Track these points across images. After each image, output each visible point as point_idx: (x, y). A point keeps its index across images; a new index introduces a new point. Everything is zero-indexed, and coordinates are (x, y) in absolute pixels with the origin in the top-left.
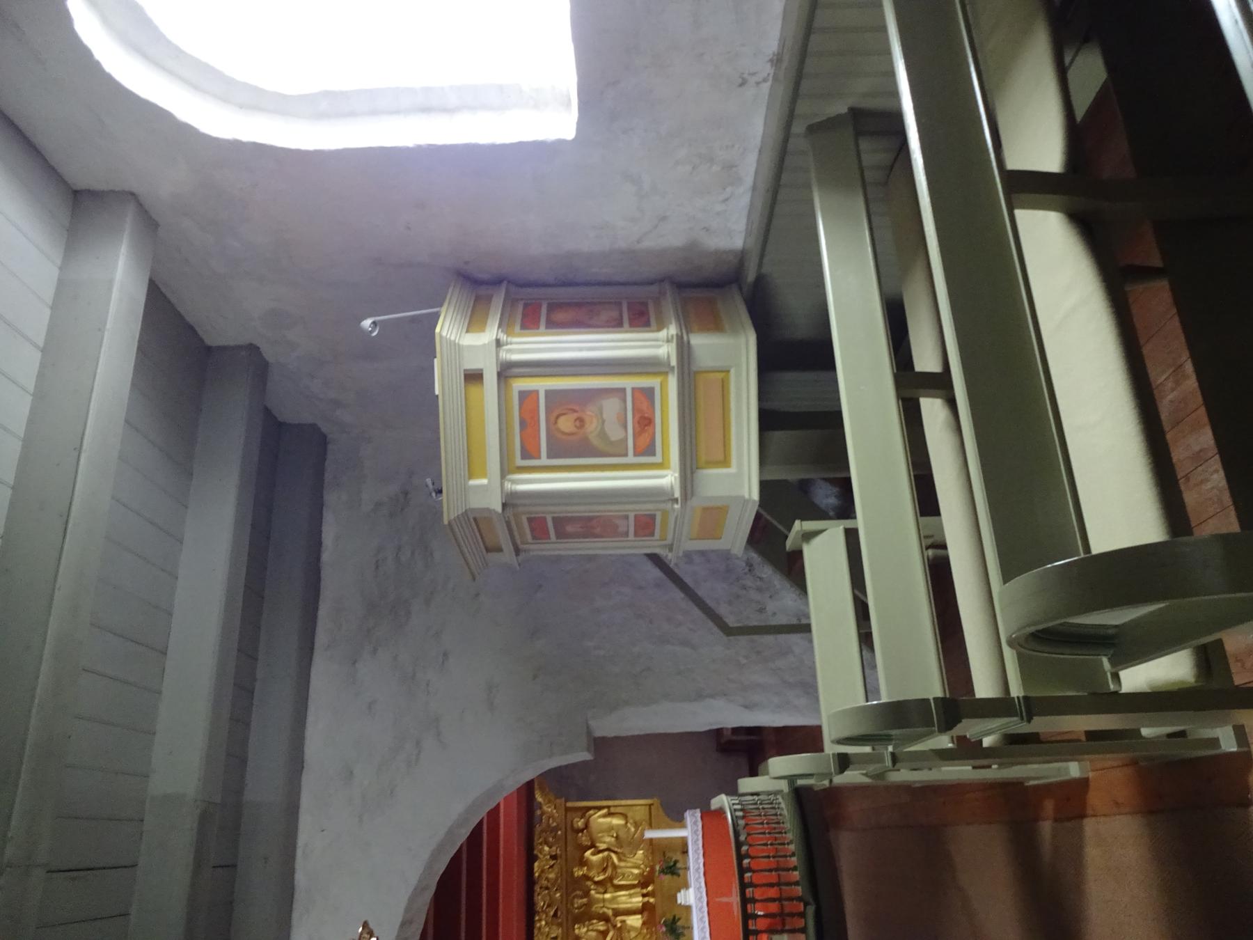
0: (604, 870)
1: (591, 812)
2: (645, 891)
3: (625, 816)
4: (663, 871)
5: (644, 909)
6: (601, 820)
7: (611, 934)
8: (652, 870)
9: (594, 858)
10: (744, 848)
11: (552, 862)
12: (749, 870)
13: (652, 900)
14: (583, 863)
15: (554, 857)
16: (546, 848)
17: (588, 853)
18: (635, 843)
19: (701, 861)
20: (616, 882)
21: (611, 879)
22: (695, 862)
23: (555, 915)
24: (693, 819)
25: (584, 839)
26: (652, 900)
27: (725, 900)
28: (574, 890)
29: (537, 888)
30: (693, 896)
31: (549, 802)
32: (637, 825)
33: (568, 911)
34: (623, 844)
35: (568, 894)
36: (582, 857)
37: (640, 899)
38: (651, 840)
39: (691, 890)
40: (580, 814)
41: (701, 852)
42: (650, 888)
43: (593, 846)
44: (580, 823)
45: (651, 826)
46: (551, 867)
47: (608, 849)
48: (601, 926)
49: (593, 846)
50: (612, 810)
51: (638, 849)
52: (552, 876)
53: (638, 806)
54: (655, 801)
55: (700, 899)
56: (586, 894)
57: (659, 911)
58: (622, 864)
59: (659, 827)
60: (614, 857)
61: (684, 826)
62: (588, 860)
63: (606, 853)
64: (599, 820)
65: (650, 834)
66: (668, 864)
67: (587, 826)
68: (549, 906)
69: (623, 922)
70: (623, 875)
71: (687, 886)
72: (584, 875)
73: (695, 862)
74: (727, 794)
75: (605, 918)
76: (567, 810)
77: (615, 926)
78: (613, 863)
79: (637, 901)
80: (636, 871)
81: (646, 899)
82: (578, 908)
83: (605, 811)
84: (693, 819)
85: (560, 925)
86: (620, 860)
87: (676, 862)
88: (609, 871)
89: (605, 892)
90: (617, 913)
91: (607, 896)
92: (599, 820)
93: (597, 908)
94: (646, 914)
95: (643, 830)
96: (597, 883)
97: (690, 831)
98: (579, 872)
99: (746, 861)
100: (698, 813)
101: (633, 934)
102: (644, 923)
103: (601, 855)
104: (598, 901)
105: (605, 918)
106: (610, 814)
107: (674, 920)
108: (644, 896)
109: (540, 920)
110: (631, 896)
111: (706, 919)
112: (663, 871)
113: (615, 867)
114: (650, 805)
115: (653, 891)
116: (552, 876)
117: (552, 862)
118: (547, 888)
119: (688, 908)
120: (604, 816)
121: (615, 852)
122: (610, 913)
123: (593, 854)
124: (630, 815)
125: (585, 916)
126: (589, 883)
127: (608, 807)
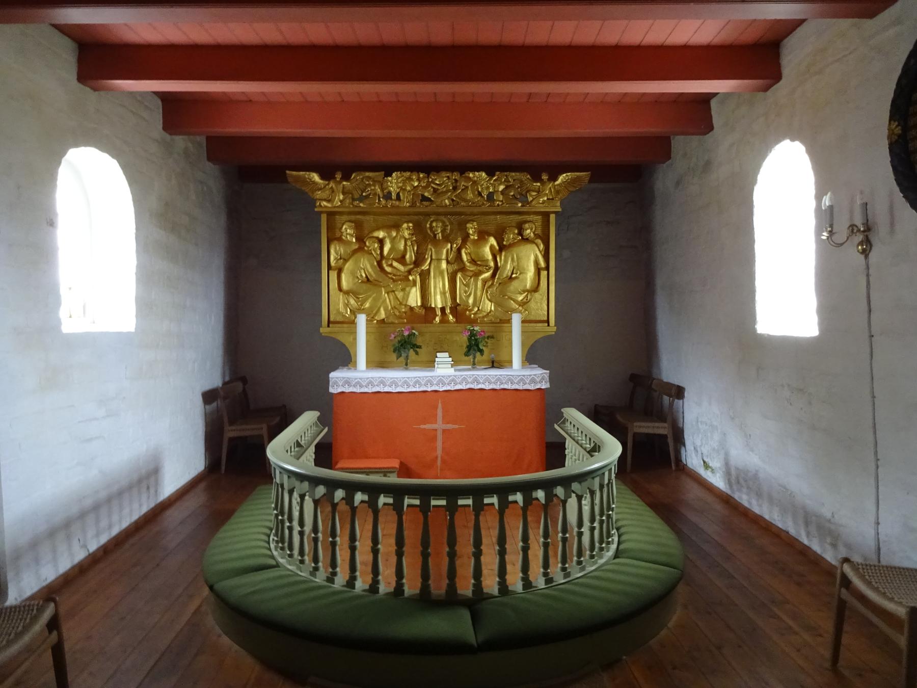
0: (473, 262)
1: (542, 247)
2: (448, 311)
3: (535, 289)
4: (472, 334)
5: (428, 310)
6: (532, 258)
7: (401, 268)
8: (473, 322)
9: (487, 250)
10: (540, 494)
11: (485, 194)
12: (504, 504)
13: (437, 319)
14: (483, 235)
15: (490, 196)
16: (502, 188)
17: (492, 241)
18: (500, 300)
19: (487, 386)
20: (459, 275)
21: (463, 269)
22: (484, 378)
23: (425, 199)
24: (537, 378)
25: (511, 236)
26: (437, 319)
27: (449, 426)
28: (451, 223)
29: (456, 175)
30: (445, 373)
31: (558, 192)
32: (523, 304)
33: (428, 215)
34: (500, 283)
35: (446, 214)
36: (490, 235)
37: (440, 306)
38: (509, 321)
39: (451, 371)
40: (539, 232)
41: (497, 387)
42: (451, 317)
43: (502, 248)
44: (528, 232)
45: (523, 322)
46: (480, 194)
47: (497, 268)
48: (410, 256)
49: (502, 248)
50: (544, 274)
51: (498, 304)
52: (470, 195)
53: (544, 305)
54: (552, 328)
55: (441, 382)
56: (447, 239)
57: (424, 327)
58: (480, 284)
59: (524, 332)
60: (487, 275)
61: (523, 366)
62: (486, 241)
63: (492, 264)
64: (529, 257)
65: (516, 319)
66: (479, 345)
67: (526, 240)
68: (435, 190)
69: (414, 283)
70: (467, 285)
71: (455, 363)
72: (468, 235)
73: (484, 378)
74: (622, 459)
75: (418, 263)
76: (546, 215)
77: (409, 272)
78: (481, 273)
79: (437, 301)
80: (471, 301)
81: (439, 312)
82: (431, 227)
83: (542, 264)
84: (537, 378)
85: (413, 205)
86: (485, 282)
87: (481, 351)
88: (473, 268)
89: (448, 262)
90: (425, 276)
91: (444, 265)
92: (529, 257)
93: (431, 251)
94: (423, 312)
95: (520, 312)
96: (459, 251)
97: (519, 374)
98: (471, 229)
99: (519, 497)
100: (545, 385)
101: (400, 295)
102: (412, 309)
103: (490, 257)
104: (439, 253)
105: (418, 263)
106: (538, 270)
107: (415, 347)
108: (443, 309)
109: (419, 180)
110: (443, 293)
111: (417, 389)
112: (472, 334)
113: (477, 275)
114: (548, 321)
115: (448, 322)
116: (470, 195)
117: (485, 194)
118: (455, 188)
119: (430, 363)
120: (536, 263)
121: (493, 275)
122: (425, 267)
123: (492, 247)
124: (537, 295)
125: (424, 238)
126: (459, 241)
127: (547, 268)
